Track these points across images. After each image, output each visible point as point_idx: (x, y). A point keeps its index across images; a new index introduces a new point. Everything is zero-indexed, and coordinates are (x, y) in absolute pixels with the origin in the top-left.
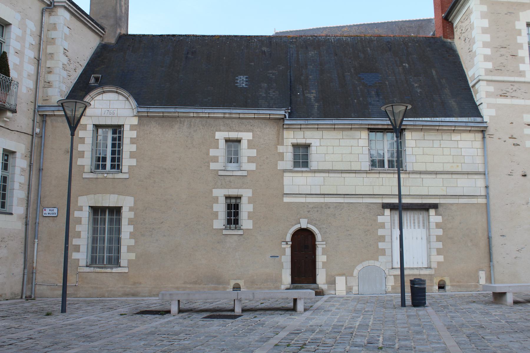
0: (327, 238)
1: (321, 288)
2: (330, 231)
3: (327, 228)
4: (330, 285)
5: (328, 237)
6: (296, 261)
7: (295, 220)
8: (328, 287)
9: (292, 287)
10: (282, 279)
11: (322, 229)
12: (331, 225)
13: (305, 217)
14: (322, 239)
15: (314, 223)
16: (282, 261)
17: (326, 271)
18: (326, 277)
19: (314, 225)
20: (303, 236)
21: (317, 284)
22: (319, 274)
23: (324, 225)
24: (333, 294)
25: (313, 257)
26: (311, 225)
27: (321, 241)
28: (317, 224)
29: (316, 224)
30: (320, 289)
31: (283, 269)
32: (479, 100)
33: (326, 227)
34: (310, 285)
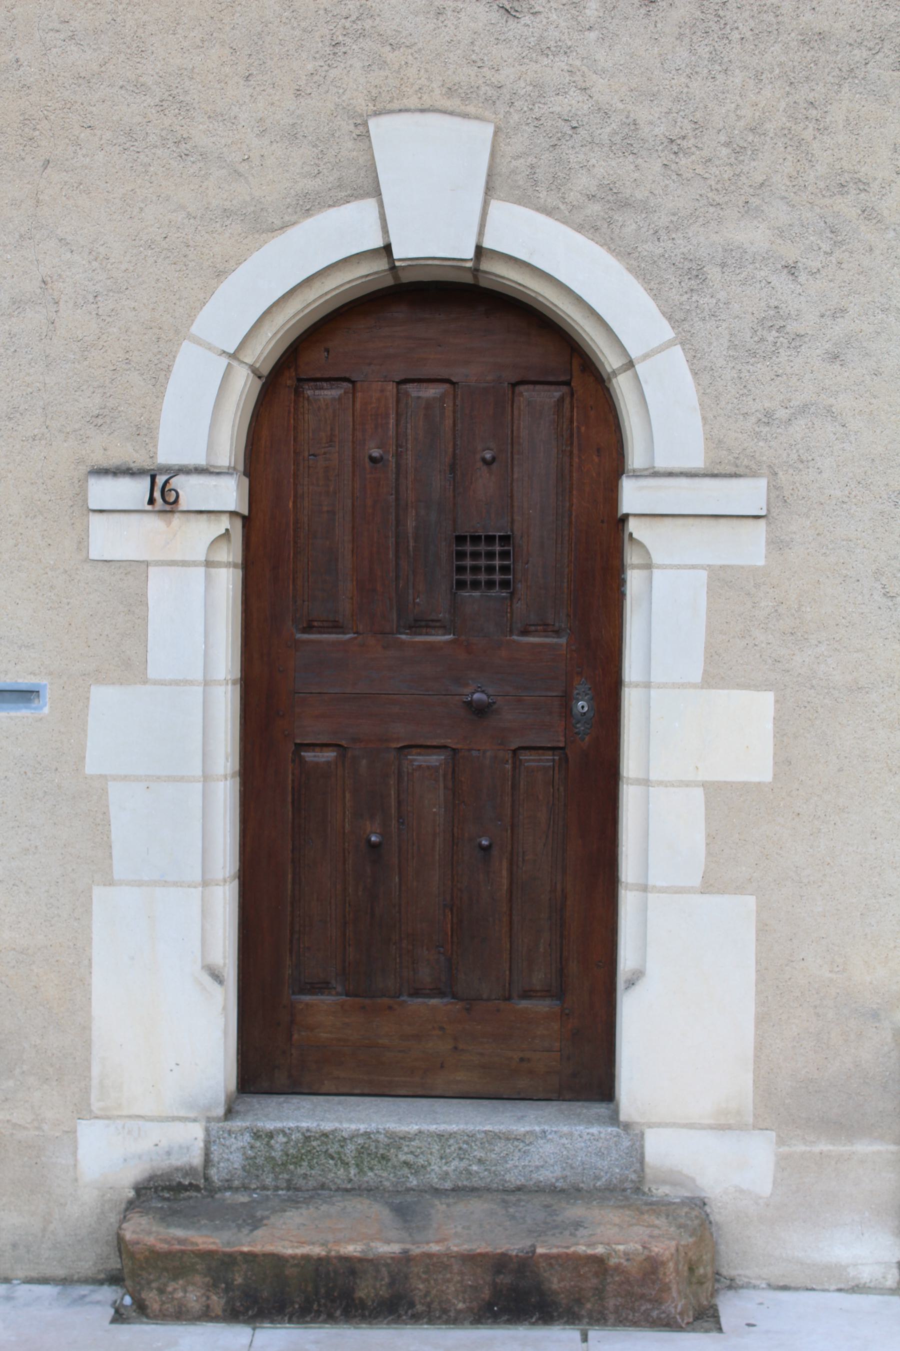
0: (799, 427)
1: (673, 1178)
2: (839, 312)
3: (792, 270)
4: (824, 1147)
5: (804, 409)
6: (329, 755)
7: (292, 135)
8: (783, 1163)
9: (238, 1160)
10: (86, 1028)
11: (713, 272)
12: (868, 213)
13: (450, 92)
14: (713, 441)
15: (583, 182)
16: (91, 768)
17: (763, 929)
18: (761, 1019)
19: (595, 208)
20: (431, 392)
21: (614, 1119)
22: (653, 969)
23: (748, 210)
24: (866, 1274)
25: (582, 706)
26: (548, 212)
27: (698, 462)
28: (640, 194)
29: (625, 204)
30: (661, 1191)
31: (111, 883)
32: (210, 347)
33: (790, 252)
34: (508, 1138)
